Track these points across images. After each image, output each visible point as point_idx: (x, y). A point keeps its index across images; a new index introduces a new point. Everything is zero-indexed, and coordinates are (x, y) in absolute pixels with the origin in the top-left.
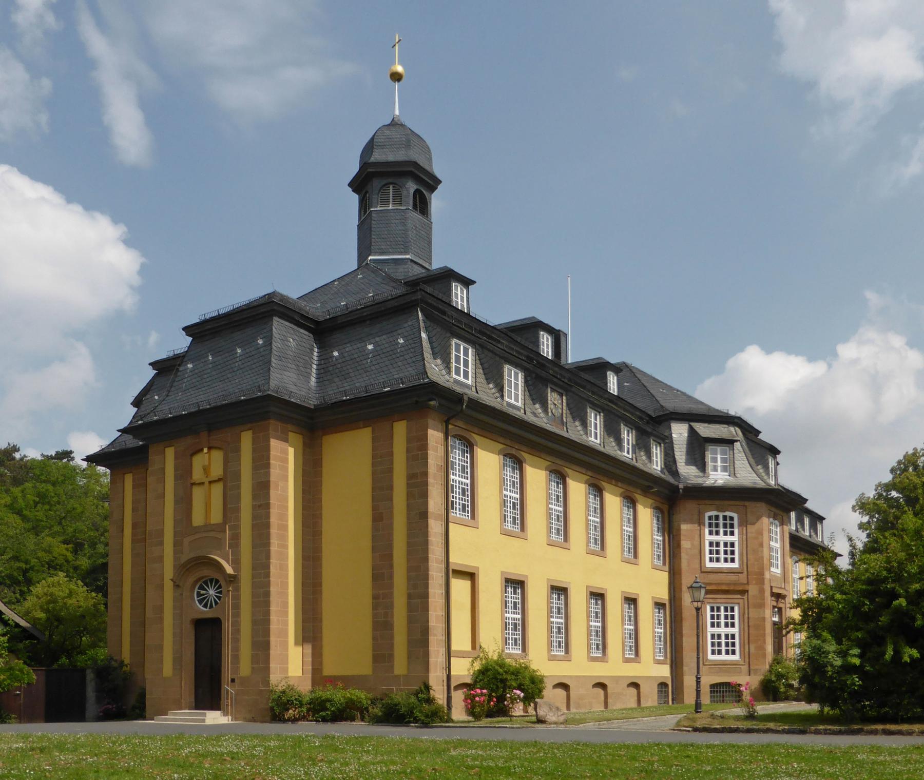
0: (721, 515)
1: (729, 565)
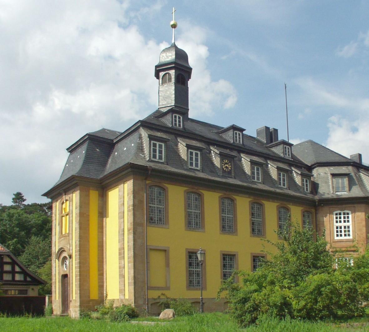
0: (342, 212)
1: (347, 238)
